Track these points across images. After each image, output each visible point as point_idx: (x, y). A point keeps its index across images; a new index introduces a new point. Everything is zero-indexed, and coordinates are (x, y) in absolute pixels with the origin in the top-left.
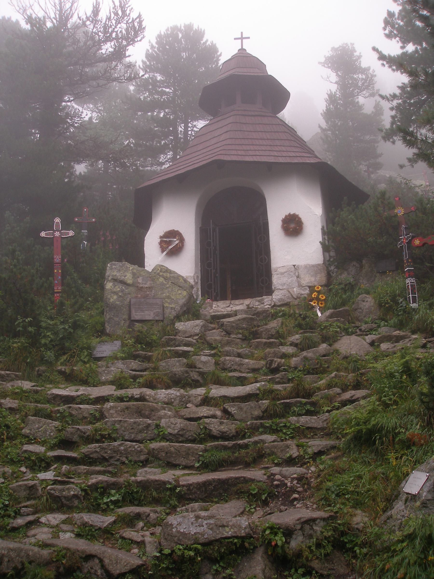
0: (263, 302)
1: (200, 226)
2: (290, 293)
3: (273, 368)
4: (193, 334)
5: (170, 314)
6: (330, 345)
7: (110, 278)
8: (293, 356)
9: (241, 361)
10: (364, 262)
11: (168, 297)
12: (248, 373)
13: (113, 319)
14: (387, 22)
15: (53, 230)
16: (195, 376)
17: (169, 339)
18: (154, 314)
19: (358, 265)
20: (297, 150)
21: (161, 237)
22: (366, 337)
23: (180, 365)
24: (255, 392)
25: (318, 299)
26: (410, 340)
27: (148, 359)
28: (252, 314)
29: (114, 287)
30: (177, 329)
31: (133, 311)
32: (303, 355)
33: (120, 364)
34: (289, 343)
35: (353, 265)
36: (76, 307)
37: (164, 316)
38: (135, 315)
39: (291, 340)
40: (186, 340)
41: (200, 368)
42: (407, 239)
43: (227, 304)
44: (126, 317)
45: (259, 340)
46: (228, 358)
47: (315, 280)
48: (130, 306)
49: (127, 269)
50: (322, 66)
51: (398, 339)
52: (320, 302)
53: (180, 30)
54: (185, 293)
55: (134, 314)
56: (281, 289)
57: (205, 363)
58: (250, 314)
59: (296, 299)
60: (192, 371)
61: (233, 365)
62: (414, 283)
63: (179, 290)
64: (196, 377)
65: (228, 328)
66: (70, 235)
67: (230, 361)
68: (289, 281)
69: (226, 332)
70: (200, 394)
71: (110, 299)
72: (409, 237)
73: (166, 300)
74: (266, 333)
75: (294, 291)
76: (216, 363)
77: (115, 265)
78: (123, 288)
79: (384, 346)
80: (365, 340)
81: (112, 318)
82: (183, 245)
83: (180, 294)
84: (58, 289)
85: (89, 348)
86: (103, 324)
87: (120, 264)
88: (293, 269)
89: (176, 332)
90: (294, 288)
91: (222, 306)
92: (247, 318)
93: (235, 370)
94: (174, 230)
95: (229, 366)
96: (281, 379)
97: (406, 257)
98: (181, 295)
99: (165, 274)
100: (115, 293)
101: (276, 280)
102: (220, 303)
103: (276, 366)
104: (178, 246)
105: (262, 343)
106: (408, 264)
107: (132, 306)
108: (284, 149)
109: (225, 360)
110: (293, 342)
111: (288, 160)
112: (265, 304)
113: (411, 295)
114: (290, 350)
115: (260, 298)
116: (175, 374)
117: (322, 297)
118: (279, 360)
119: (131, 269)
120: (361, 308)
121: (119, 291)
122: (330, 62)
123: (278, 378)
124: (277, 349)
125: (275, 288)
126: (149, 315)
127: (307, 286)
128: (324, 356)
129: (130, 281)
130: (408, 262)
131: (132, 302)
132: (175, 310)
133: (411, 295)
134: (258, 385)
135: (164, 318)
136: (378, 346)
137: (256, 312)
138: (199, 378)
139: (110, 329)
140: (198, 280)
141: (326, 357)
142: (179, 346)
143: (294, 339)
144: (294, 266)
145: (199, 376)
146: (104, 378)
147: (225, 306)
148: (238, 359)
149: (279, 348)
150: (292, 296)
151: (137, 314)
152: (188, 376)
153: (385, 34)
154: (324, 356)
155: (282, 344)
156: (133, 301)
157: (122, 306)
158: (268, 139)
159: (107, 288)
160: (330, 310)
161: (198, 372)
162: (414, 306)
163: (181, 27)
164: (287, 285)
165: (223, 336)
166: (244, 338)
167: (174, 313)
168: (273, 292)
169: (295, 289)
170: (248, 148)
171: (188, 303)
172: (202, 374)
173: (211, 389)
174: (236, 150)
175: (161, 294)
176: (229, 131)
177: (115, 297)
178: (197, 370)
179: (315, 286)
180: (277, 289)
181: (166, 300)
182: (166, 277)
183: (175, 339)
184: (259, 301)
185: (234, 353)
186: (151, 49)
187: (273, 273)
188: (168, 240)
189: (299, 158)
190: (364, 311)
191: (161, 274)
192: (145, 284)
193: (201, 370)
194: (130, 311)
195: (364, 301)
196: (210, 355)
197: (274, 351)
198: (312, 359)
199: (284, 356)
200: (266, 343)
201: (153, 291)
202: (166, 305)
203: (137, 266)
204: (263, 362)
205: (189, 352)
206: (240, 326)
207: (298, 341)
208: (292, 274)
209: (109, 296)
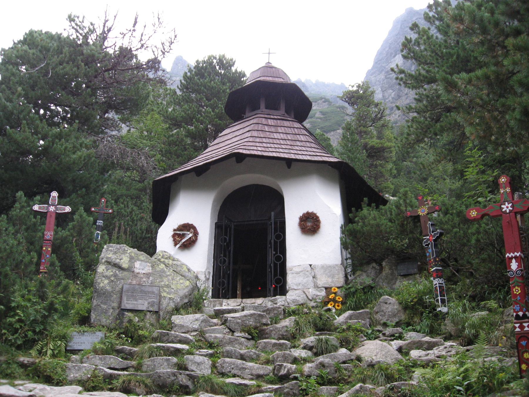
1: (216, 221)
2: (305, 294)
3: (282, 375)
4: (190, 330)
5: (167, 305)
7: (103, 261)
8: (305, 360)
9: (243, 364)
10: (384, 264)
11: (168, 286)
12: (252, 379)
13: (101, 307)
14: (404, 46)
15: (48, 204)
16: (183, 379)
17: (161, 333)
18: (149, 303)
19: (377, 267)
20: (318, 151)
21: (175, 230)
22: (392, 343)
23: (168, 365)
25: (334, 300)
26: (446, 347)
27: (129, 356)
29: (107, 270)
30: (173, 323)
31: (125, 298)
33: (97, 359)
34: (302, 346)
36: (60, 289)
37: (159, 307)
38: (127, 303)
39: (305, 342)
40: (181, 336)
41: (192, 371)
42: (433, 236)
44: (115, 305)
46: (227, 360)
47: (332, 282)
48: (121, 291)
49: (124, 252)
51: (430, 346)
52: (337, 304)
54: (187, 283)
55: (125, 302)
56: (296, 290)
58: (259, 311)
59: (311, 300)
60: (181, 374)
61: (233, 369)
62: (442, 284)
63: (182, 279)
65: (233, 326)
66: (66, 211)
67: (230, 363)
68: (305, 280)
71: (99, 284)
72: (437, 234)
73: (165, 288)
74: (276, 333)
75: (309, 292)
76: (214, 366)
77: (111, 247)
81: (99, 305)
82: (196, 239)
84: (44, 269)
85: (64, 337)
86: (89, 311)
87: (118, 246)
89: (171, 326)
92: (254, 314)
93: (234, 376)
94: (188, 224)
95: (228, 370)
96: (291, 389)
97: (433, 255)
98: (182, 285)
99: (166, 261)
100: (106, 277)
101: (291, 280)
103: (285, 372)
105: (271, 344)
107: (124, 293)
109: (224, 362)
111: (309, 158)
113: (439, 298)
115: (273, 298)
116: (160, 377)
117: (339, 299)
118: (289, 365)
119: (128, 252)
120: (383, 311)
121: (112, 275)
123: (287, 388)
126: (142, 305)
128: (344, 362)
129: (125, 265)
130: (435, 260)
131: (124, 289)
133: (439, 298)
135: (159, 309)
136: (407, 354)
138: (189, 383)
139: (96, 318)
140: (209, 276)
142: (173, 342)
143: (308, 342)
144: (310, 265)
146: (72, 375)
147: (235, 304)
148: (240, 361)
149: (290, 351)
150: (307, 297)
151: (129, 302)
154: (344, 362)
156: (126, 287)
157: (112, 292)
158: (288, 140)
159: (98, 271)
161: (188, 375)
165: (225, 334)
167: (172, 305)
168: (287, 292)
169: (310, 290)
170: (269, 145)
171: (190, 295)
177: (106, 282)
178: (187, 372)
179: (331, 288)
180: (292, 289)
181: (165, 288)
183: (168, 334)
185: (236, 354)
187: (288, 271)
188: (181, 233)
190: (387, 314)
191: (162, 260)
192: (143, 269)
193: (192, 373)
195: (386, 303)
196: (205, 356)
197: (285, 354)
198: (329, 366)
199: (295, 361)
200: (275, 345)
203: (136, 250)
205: (183, 349)
206: (246, 323)
209: (99, 281)
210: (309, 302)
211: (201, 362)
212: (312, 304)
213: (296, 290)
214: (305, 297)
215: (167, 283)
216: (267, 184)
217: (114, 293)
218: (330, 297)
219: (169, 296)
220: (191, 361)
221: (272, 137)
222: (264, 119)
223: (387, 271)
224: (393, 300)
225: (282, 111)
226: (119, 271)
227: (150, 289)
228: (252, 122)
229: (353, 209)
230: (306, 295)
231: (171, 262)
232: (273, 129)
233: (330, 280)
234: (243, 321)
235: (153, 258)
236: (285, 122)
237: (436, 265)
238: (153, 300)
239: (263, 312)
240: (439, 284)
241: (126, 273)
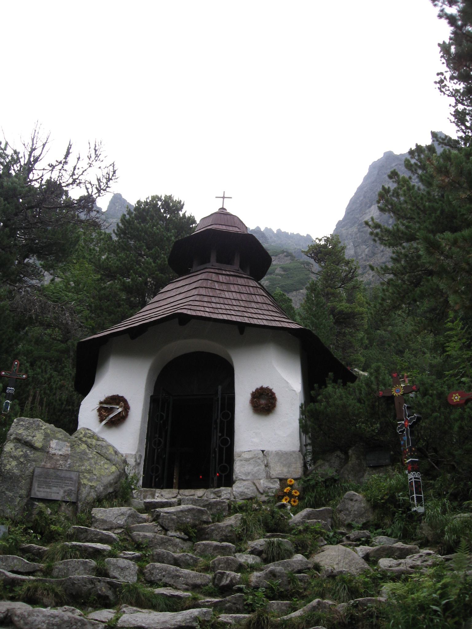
0: (220, 494)
1: (152, 394)
3: (223, 586)
4: (114, 526)
6: (307, 557)
7: (12, 437)
8: (253, 568)
9: (177, 571)
10: (350, 452)
11: (90, 472)
12: (186, 590)
13: (5, 494)
16: (103, 588)
18: (65, 492)
19: (343, 456)
21: (101, 403)
22: (358, 549)
23: (85, 569)
24: (190, 625)
25: (290, 495)
26: (421, 556)
27: (37, 556)
28: (202, 504)
29: (16, 449)
30: (94, 517)
31: (35, 485)
32: (269, 569)
34: (249, 550)
35: (337, 455)
37: (77, 497)
38: (38, 491)
39: (253, 545)
40: (103, 534)
41: (114, 578)
42: (409, 421)
43: (173, 494)
44: (23, 492)
45: (208, 542)
46: (158, 565)
47: (288, 472)
49: (38, 428)
50: (305, 254)
51: (403, 554)
52: (293, 499)
53: (160, 199)
54: (113, 469)
55: (36, 489)
56: (244, 480)
57: (123, 569)
58: (199, 506)
59: (262, 494)
60: (100, 581)
61: (164, 576)
64: (104, 590)
65: (166, 523)
67: (161, 569)
68: (255, 469)
69: (162, 526)
70: (104, 620)
71: (5, 465)
73: (85, 474)
75: (260, 484)
76: (141, 572)
77: (23, 421)
78: (28, 452)
79: (384, 562)
80: (356, 551)
83: (106, 469)
87: (31, 420)
88: (261, 455)
89: (91, 521)
90: (260, 479)
91: (168, 496)
92: (193, 509)
93: (165, 585)
95: (158, 577)
96: (234, 604)
97: (408, 444)
98: (107, 471)
99: (89, 441)
100: (15, 458)
101: (239, 468)
102: (165, 491)
103: (228, 582)
104: (121, 415)
106: (411, 454)
108: (260, 312)
109: (154, 568)
110: (256, 549)
111: (265, 323)
112: (223, 498)
114: (250, 559)
116: (73, 584)
117: (296, 493)
118: (233, 574)
119: (43, 428)
120: (347, 509)
121: (22, 455)
122: (313, 252)
123: (229, 602)
124: (232, 557)
125: (236, 477)
126: (57, 493)
127: (278, 478)
128: (299, 572)
129: (38, 444)
130: (410, 450)
131: (36, 473)
132: (96, 491)
133: (415, 495)
134: (195, 612)
137: (207, 503)
138: (110, 593)
140: (140, 461)
141: (302, 574)
143: (256, 545)
144: (263, 451)
145: (110, 589)
147: (170, 496)
148: (173, 567)
149: (235, 556)
150: (258, 489)
151: (41, 489)
152: (93, 588)
153: (378, 207)
154: (299, 572)
155: (240, 551)
156: (38, 471)
157: (21, 476)
159: (5, 449)
160: (307, 509)
162: (421, 509)
163: (161, 197)
164: (252, 475)
165: (156, 532)
166: (187, 537)
167: (93, 495)
168: (234, 482)
169: (262, 481)
171: (116, 483)
172: (113, 586)
173: (124, 612)
174: (204, 307)
175: (79, 466)
176: (198, 287)
177: (14, 463)
178: (108, 579)
179: (286, 479)
180: (240, 480)
181: (85, 474)
182: (91, 444)
183: (86, 531)
184: (214, 493)
185: (169, 558)
186: (128, 214)
187: (236, 458)
188: (109, 406)
189: (277, 323)
190: (352, 512)
191: (84, 439)
193: (114, 580)
194: (31, 484)
195: (352, 500)
197: (228, 559)
198: (281, 576)
199: (240, 568)
200: (217, 547)
201: (69, 460)
202: (84, 481)
203: (53, 425)
204: (210, 576)
205: (104, 550)
206: (183, 520)
207: (260, 549)
208: (259, 461)
209: (5, 462)
210: (259, 495)
211: (125, 567)
212: (264, 498)
213: (244, 480)
214: (256, 490)
215: (88, 467)
216: (192, 350)
217: (22, 478)
218: (285, 491)
219: (90, 484)
220: (114, 565)
221: (224, 296)
222: (214, 275)
223: (353, 461)
224: (359, 496)
225: (237, 266)
226: (31, 451)
227: (68, 475)
228: (199, 277)
229: (316, 385)
230: (257, 488)
231: (94, 442)
232: (224, 287)
233: (285, 470)
234: (178, 517)
235: (73, 437)
236: (238, 279)
237: (411, 456)
238: (70, 487)
239: (204, 506)
240: (415, 478)
241: (38, 454)
